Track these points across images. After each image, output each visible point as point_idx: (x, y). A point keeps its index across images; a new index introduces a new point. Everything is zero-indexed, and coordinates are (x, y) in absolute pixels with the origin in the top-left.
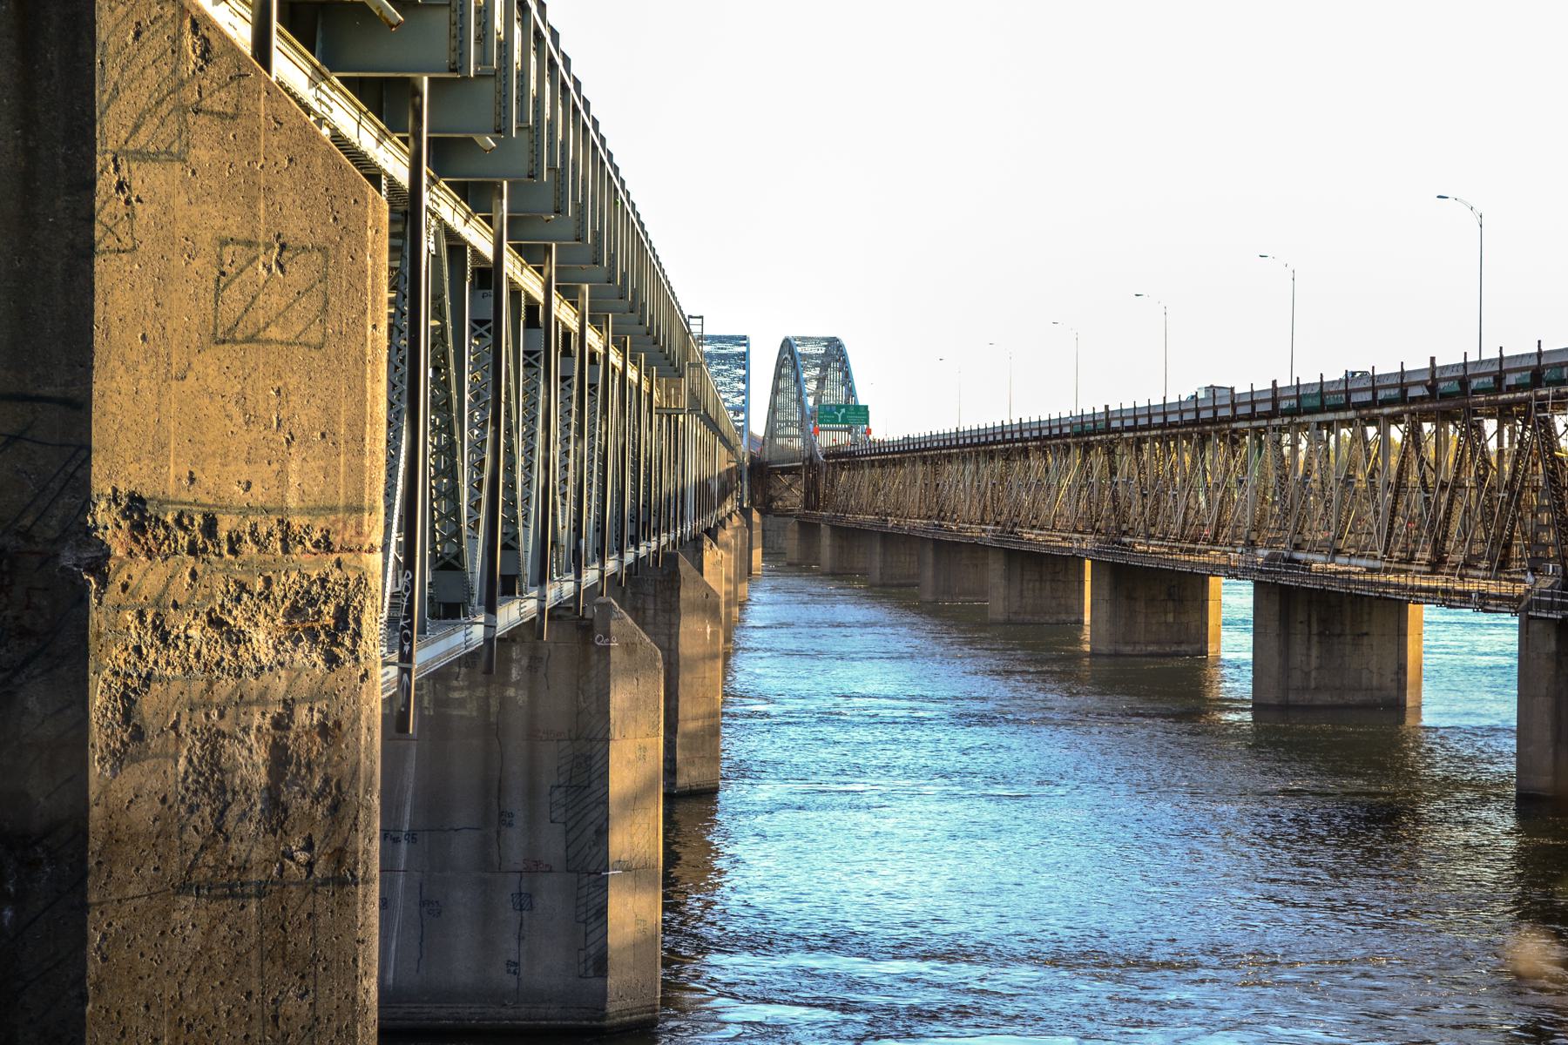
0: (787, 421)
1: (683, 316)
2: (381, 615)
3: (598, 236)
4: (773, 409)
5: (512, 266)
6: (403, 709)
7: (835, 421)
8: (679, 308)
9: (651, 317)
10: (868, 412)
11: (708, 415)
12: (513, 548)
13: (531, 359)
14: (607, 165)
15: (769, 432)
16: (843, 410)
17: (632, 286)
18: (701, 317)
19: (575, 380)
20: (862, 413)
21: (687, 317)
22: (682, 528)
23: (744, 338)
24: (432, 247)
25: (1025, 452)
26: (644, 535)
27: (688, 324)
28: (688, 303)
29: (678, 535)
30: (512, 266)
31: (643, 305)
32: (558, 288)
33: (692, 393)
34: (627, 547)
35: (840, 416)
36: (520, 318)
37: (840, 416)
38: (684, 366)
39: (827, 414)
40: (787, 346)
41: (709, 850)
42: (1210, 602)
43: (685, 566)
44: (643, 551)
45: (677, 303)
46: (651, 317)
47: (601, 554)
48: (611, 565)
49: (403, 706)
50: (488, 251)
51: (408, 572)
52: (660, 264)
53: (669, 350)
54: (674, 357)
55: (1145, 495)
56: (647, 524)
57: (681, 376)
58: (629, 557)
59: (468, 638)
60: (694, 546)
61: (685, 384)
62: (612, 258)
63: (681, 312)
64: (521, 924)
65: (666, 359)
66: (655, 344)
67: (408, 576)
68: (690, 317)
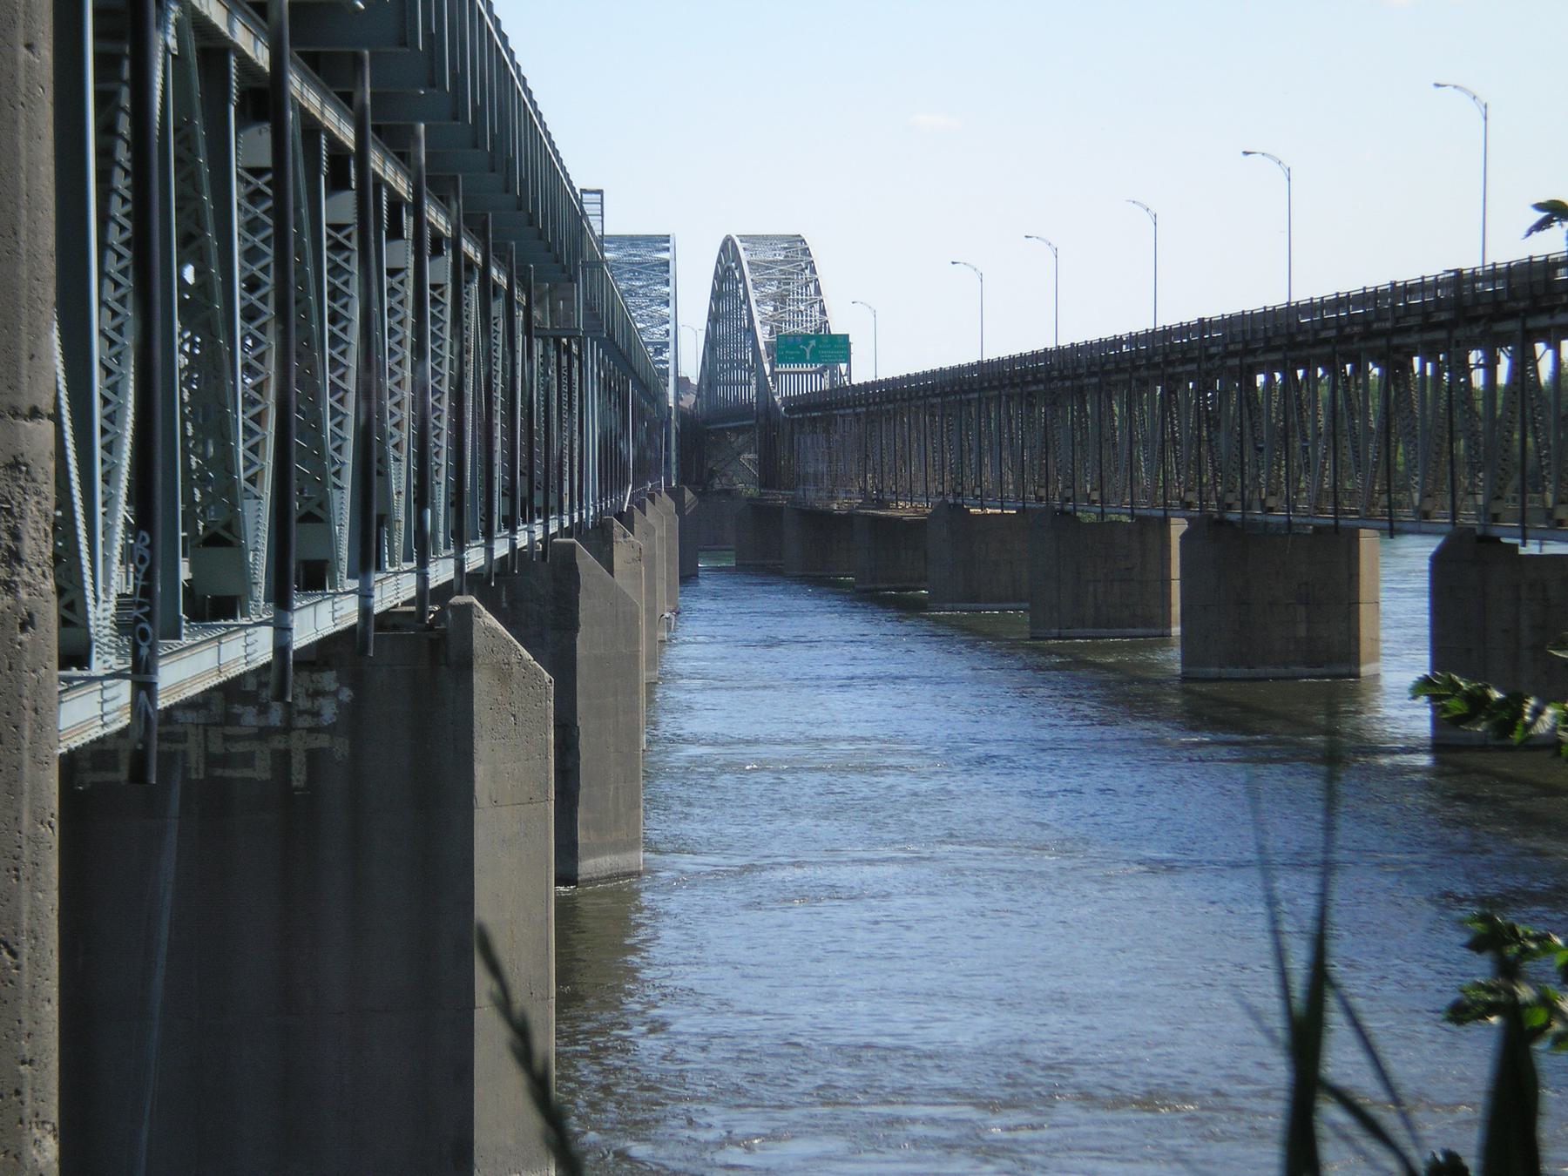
0: (732, 361)
1: (573, 189)
2: (106, 606)
3: (433, 40)
4: (711, 343)
5: (302, 91)
6: (140, 747)
7: (800, 359)
8: (567, 175)
9: (523, 183)
10: (849, 345)
11: (615, 344)
12: (318, 520)
13: (340, 237)
14: (487, 18)
15: (705, 381)
16: (813, 343)
17: (492, 128)
18: (600, 192)
19: (411, 273)
20: (839, 347)
21: (578, 192)
22: (581, 508)
23: (666, 239)
24: (172, 43)
25: (1080, 392)
26: (523, 515)
27: (581, 203)
28: (580, 170)
29: (576, 521)
30: (302, 91)
31: (510, 163)
32: (377, 129)
33: (589, 306)
34: (499, 531)
35: (808, 351)
36: (318, 170)
37: (808, 351)
38: (576, 266)
39: (789, 348)
40: (728, 249)
41: (631, 973)
42: (1362, 607)
43: (586, 560)
44: (522, 540)
45: (564, 169)
46: (523, 183)
47: (459, 539)
48: (475, 558)
49: (141, 741)
50: (261, 56)
51: (143, 533)
52: (534, 104)
53: (553, 238)
54: (545, 222)
55: (1261, 450)
56: (528, 500)
57: (573, 279)
58: (501, 549)
59: (249, 650)
60: (599, 538)
61: (579, 292)
62: (458, 79)
63: (570, 183)
64: (750, 1013)
65: (564, 272)
66: (520, 209)
67: (144, 539)
68: (583, 191)
